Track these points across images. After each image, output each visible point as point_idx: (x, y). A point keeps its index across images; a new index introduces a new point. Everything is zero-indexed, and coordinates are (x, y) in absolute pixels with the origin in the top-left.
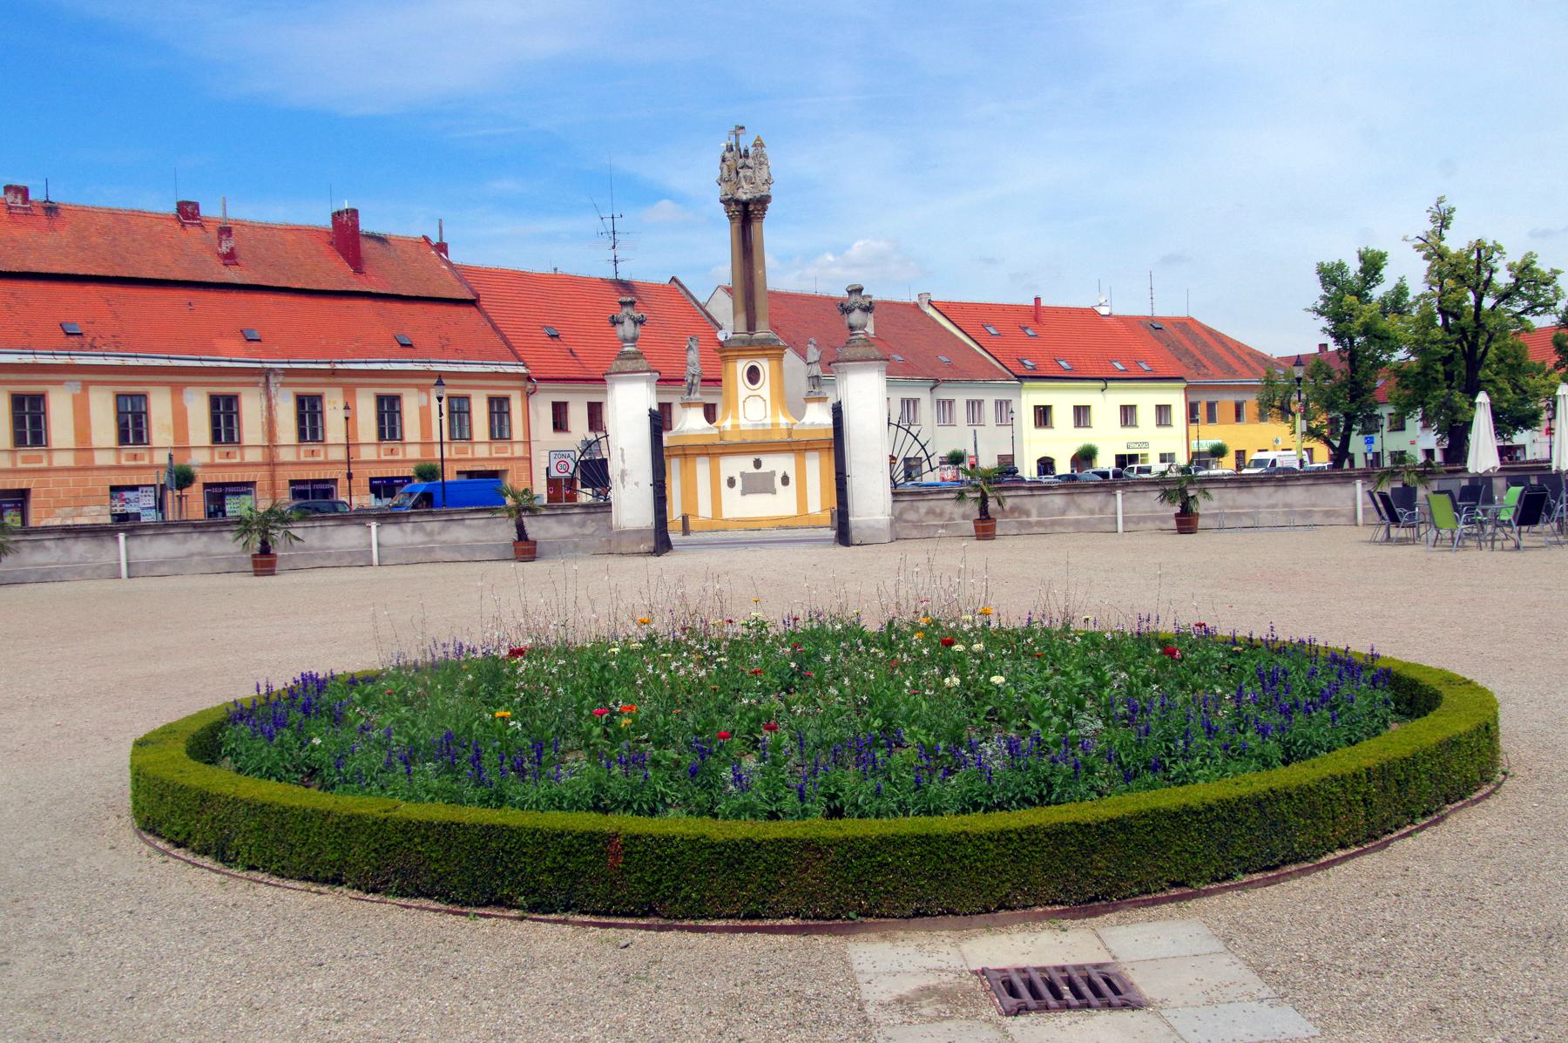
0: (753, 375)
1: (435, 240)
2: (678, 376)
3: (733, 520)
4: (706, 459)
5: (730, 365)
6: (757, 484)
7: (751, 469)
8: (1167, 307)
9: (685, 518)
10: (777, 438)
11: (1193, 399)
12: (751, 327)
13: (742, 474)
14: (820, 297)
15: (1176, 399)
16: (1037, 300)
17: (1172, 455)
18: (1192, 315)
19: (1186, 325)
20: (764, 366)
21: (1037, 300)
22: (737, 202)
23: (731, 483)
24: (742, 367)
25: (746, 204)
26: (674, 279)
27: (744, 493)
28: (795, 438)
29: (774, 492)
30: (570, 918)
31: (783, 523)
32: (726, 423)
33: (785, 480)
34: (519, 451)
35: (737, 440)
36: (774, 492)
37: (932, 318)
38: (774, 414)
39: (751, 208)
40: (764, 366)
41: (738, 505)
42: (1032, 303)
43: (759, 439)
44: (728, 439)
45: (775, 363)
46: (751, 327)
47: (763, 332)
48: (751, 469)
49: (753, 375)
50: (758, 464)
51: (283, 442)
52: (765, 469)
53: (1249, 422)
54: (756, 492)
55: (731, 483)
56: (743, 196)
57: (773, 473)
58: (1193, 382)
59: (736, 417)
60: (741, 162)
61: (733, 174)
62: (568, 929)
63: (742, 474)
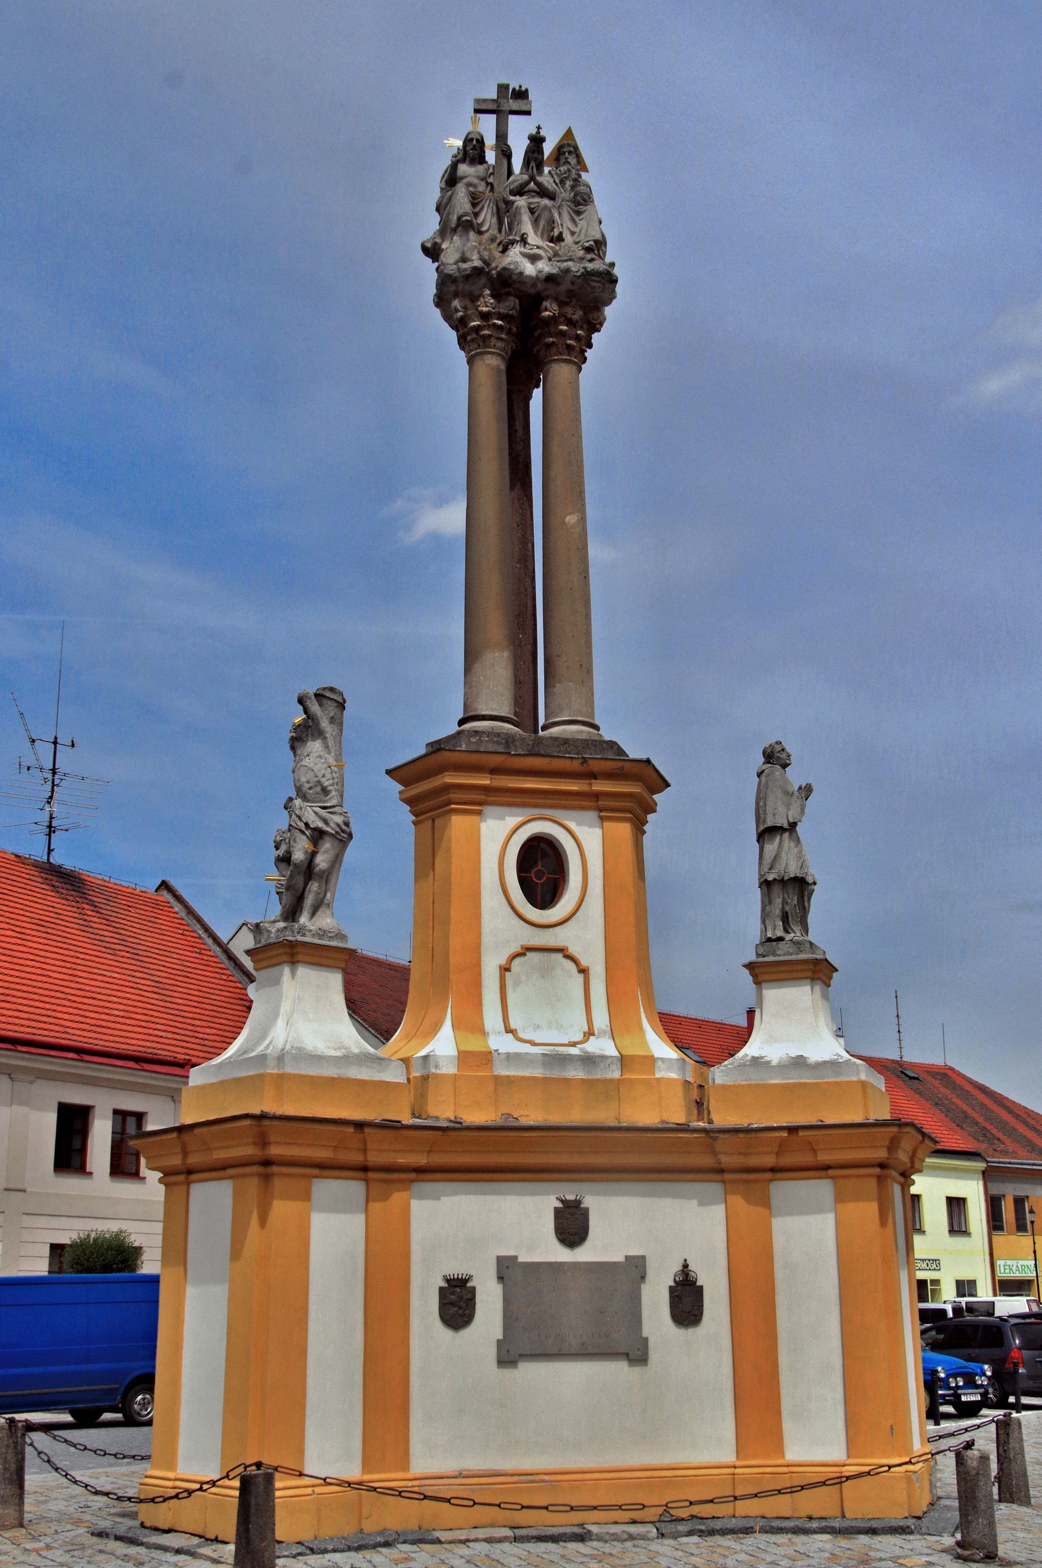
0: (541, 871)
4: (354, 1188)
5: (458, 823)
6: (565, 1317)
10: (647, 1117)
11: (996, 1189)
15: (973, 1191)
17: (972, 1283)
20: (586, 842)
22: (505, 283)
23: (457, 1303)
24: (496, 837)
26: (164, 885)
28: (723, 1117)
33: (687, 1302)
39: (549, 310)
40: (586, 842)
45: (624, 830)
49: (541, 871)
50: (572, 1226)
52: (602, 1246)
53: (1009, 1233)
56: (528, 260)
57: (636, 1269)
58: (995, 1160)
59: (470, 1023)
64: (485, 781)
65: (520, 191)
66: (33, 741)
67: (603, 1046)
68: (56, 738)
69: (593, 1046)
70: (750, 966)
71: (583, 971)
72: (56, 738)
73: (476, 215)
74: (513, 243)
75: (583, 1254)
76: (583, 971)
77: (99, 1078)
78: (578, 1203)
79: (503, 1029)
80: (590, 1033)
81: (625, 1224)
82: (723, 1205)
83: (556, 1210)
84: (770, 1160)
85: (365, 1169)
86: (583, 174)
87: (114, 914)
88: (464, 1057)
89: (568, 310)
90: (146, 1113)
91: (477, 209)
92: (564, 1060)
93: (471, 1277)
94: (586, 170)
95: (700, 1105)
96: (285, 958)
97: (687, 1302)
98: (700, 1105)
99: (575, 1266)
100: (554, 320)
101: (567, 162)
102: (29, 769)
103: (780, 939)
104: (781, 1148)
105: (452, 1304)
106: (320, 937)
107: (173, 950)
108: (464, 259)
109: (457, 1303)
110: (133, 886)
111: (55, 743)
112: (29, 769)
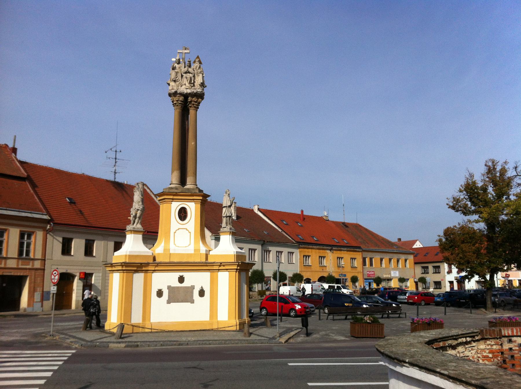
0: (183, 214)
1: (11, 146)
6: (180, 295)
7: (176, 284)
8: (349, 220)
10: (198, 260)
12: (183, 181)
13: (169, 287)
14: (214, 203)
16: (302, 211)
18: (358, 223)
19: (357, 226)
21: (302, 211)
23: (160, 294)
24: (176, 206)
25: (186, 96)
27: (169, 302)
28: (210, 260)
29: (192, 302)
32: (159, 249)
33: (202, 293)
34: (37, 265)
36: (192, 302)
38: (196, 242)
39: (190, 99)
42: (300, 213)
46: (183, 181)
48: (176, 284)
49: (183, 214)
50: (181, 280)
51: (40, 261)
54: (178, 301)
56: (185, 89)
57: (193, 287)
60: (184, 70)
63: (169, 287)
64: (171, 197)
65: (186, 73)
77: (26, 250)
81: (196, 279)
82: (44, 290)
84: (218, 268)
86: (467, 280)
89: (194, 99)
94: (469, 281)
95: (207, 258)
97: (202, 293)
98: (207, 258)
100: (191, 102)
104: (220, 266)
108: (173, 89)
109: (160, 294)
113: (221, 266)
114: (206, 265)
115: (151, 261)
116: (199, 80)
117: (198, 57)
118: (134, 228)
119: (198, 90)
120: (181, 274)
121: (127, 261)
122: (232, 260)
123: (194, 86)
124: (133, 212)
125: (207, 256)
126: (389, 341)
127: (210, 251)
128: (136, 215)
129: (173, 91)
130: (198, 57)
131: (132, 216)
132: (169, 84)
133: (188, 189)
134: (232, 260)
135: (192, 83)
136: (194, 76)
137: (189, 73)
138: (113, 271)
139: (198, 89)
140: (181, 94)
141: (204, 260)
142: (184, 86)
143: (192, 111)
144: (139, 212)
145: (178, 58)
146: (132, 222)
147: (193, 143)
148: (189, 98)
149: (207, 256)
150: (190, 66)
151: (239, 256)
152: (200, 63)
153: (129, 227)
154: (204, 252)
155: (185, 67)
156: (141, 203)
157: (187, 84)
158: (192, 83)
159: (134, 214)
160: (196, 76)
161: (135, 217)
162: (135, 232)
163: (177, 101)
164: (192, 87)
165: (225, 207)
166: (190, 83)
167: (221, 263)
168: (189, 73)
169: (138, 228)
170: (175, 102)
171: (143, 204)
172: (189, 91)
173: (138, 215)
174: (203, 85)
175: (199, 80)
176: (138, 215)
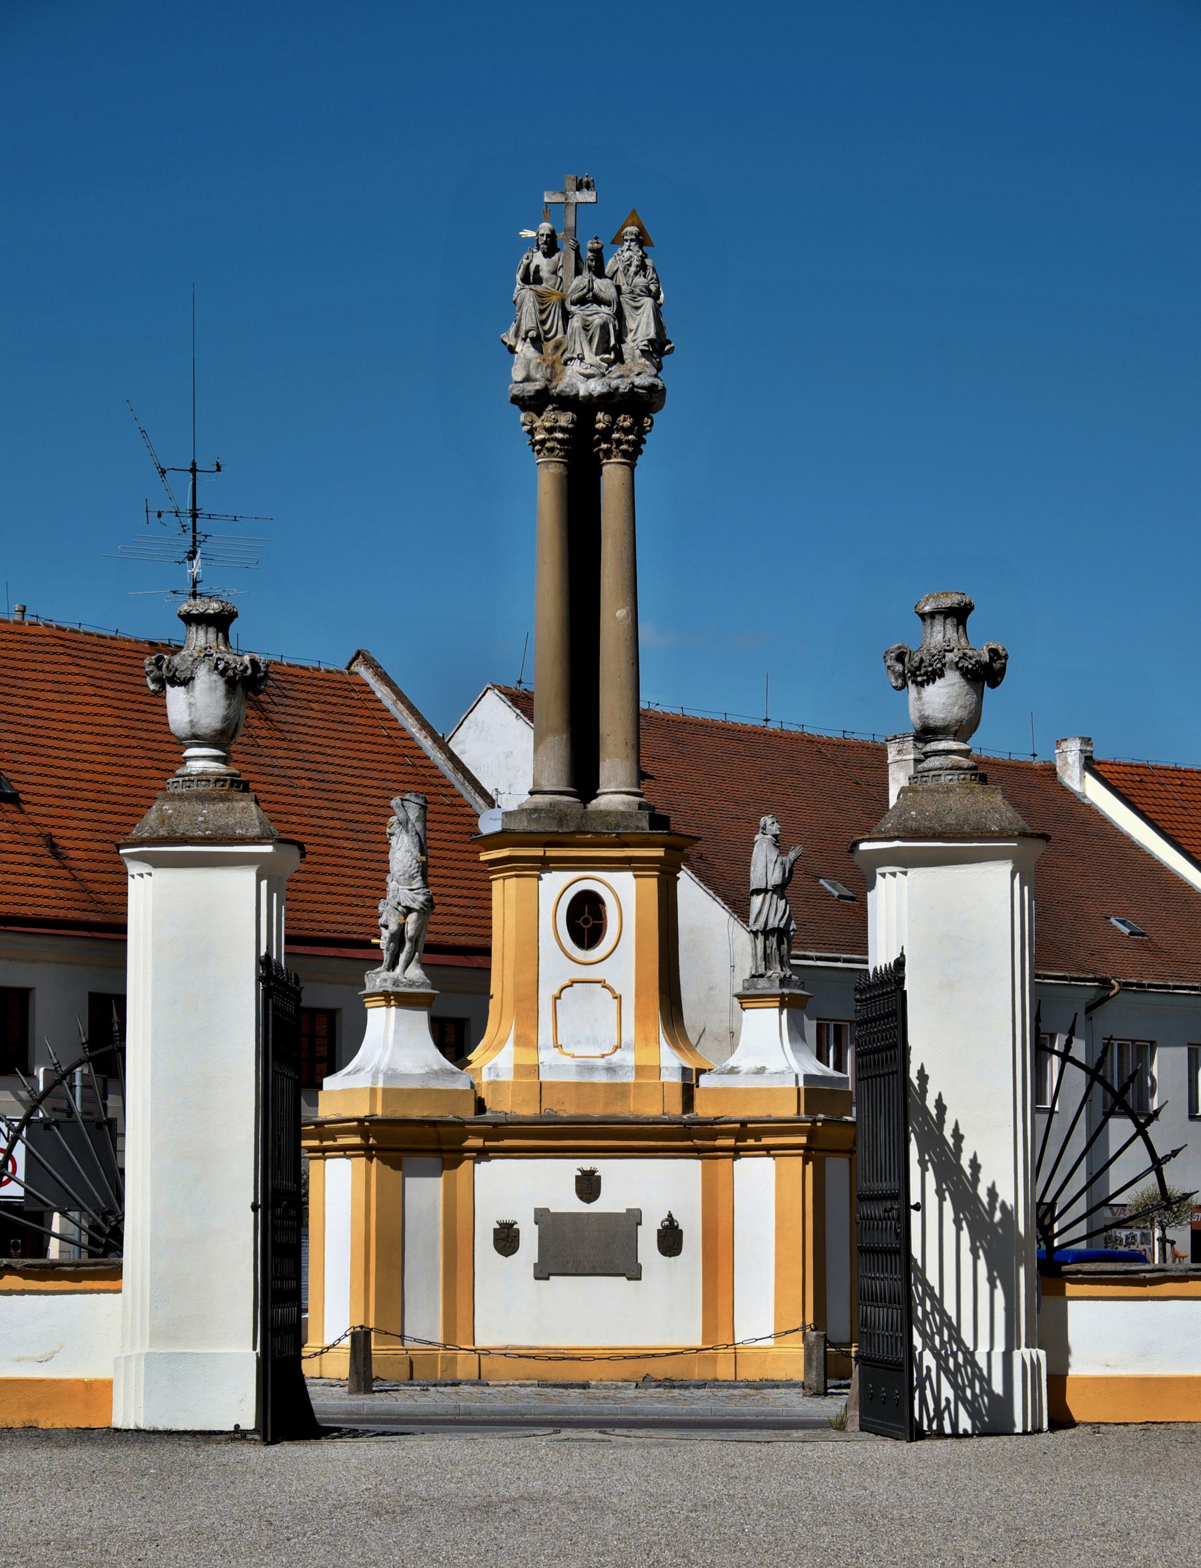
0: (586, 922)
2: (357, 933)
3: (506, 1353)
6: (586, 1247)
7: (570, 1203)
9: (360, 1340)
10: (652, 1110)
12: (583, 776)
13: (542, 1217)
14: (781, 737)
20: (624, 893)
23: (506, 1239)
24: (557, 888)
27: (542, 1272)
28: (704, 1109)
29: (635, 1274)
30: (536, 1432)
31: (658, 1369)
32: (495, 1062)
35: (528, 1110)
36: (635, 1274)
37: (1093, 812)
38: (643, 1039)
39: (602, 420)
41: (522, 1311)
43: (597, 1110)
44: (503, 1105)
46: (583, 776)
47: (614, 794)
49: (586, 922)
50: (588, 1186)
55: (506, 1239)
56: (582, 377)
57: (634, 1218)
59: (527, 1040)
60: (577, 284)
61: (555, 320)
62: (382, 1445)
63: (542, 1217)
64: (538, 852)
65: (582, 301)
66: (163, 472)
67: (627, 1058)
68: (194, 464)
69: (616, 1058)
70: (740, 997)
71: (618, 998)
72: (194, 464)
73: (543, 322)
74: (571, 359)
75: (595, 1207)
76: (618, 998)
78: (592, 1172)
79: (552, 1044)
80: (617, 1047)
81: (648, 1187)
83: (577, 1177)
85: (440, 1151)
87: (290, 719)
88: (518, 1069)
90: (339, 1009)
91: (544, 316)
92: (591, 1069)
93: (515, 1223)
96: (383, 1003)
99: (589, 1215)
100: (606, 434)
101: (629, 249)
102: (159, 516)
103: (762, 976)
105: (502, 1239)
106: (411, 986)
107: (373, 765)
108: (528, 379)
109: (670, 1239)
110: (316, 665)
111: (194, 470)
112: (159, 516)
113: (747, 1137)
114: (696, 1134)
115: (469, 1114)
116: (641, 326)
117: (634, 213)
118: (396, 983)
119: (638, 381)
120: (587, 1164)
121: (379, 1112)
122: (788, 1109)
123: (620, 359)
124: (389, 918)
125: (688, 1092)
126: (109, 906)
127: (700, 1072)
128: (402, 927)
129: (532, 388)
130: (634, 213)
131: (386, 934)
132: (512, 350)
133: (604, 814)
134: (788, 1109)
135: (611, 344)
136: (620, 315)
137: (598, 300)
138: (325, 1150)
139: (637, 373)
140: (567, 402)
141: (675, 1108)
142: (575, 366)
143: (612, 474)
144: (412, 917)
145: (545, 227)
146: (386, 956)
147: (621, 613)
148: (600, 416)
149: (688, 1092)
150: (599, 272)
151: (815, 1093)
152: (641, 240)
153: (378, 979)
154: (677, 1079)
155: (578, 272)
156: (417, 883)
157: (591, 358)
158: (611, 344)
159: (393, 927)
160: (627, 310)
161: (399, 938)
162: (404, 1000)
163: (550, 430)
164: (611, 363)
165: (757, 892)
166: (603, 348)
167: (744, 1123)
168: (598, 300)
169: (412, 984)
170: (538, 437)
171: (426, 885)
172: (595, 387)
173: (410, 929)
174: (657, 349)
175: (641, 326)
176: (410, 929)
